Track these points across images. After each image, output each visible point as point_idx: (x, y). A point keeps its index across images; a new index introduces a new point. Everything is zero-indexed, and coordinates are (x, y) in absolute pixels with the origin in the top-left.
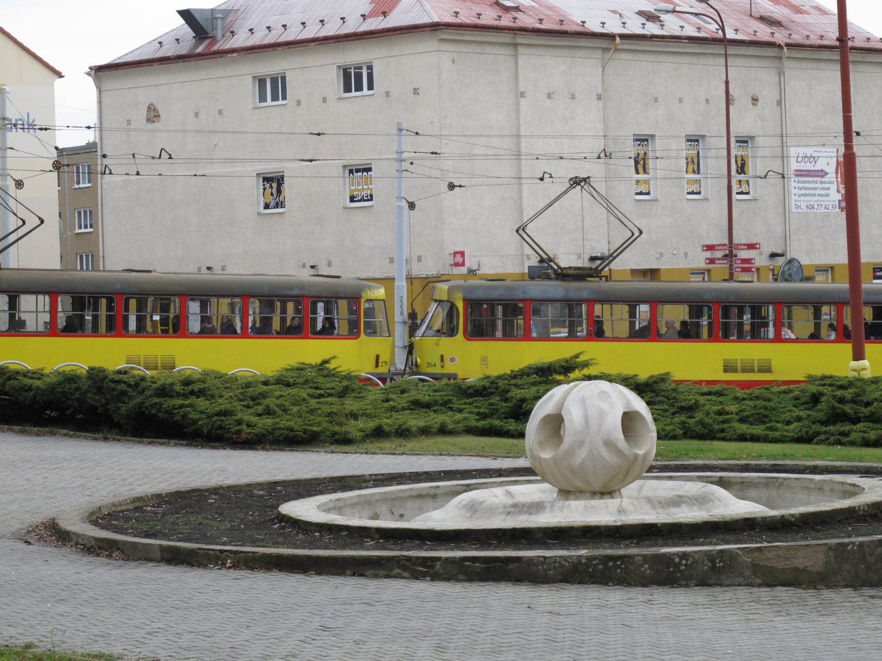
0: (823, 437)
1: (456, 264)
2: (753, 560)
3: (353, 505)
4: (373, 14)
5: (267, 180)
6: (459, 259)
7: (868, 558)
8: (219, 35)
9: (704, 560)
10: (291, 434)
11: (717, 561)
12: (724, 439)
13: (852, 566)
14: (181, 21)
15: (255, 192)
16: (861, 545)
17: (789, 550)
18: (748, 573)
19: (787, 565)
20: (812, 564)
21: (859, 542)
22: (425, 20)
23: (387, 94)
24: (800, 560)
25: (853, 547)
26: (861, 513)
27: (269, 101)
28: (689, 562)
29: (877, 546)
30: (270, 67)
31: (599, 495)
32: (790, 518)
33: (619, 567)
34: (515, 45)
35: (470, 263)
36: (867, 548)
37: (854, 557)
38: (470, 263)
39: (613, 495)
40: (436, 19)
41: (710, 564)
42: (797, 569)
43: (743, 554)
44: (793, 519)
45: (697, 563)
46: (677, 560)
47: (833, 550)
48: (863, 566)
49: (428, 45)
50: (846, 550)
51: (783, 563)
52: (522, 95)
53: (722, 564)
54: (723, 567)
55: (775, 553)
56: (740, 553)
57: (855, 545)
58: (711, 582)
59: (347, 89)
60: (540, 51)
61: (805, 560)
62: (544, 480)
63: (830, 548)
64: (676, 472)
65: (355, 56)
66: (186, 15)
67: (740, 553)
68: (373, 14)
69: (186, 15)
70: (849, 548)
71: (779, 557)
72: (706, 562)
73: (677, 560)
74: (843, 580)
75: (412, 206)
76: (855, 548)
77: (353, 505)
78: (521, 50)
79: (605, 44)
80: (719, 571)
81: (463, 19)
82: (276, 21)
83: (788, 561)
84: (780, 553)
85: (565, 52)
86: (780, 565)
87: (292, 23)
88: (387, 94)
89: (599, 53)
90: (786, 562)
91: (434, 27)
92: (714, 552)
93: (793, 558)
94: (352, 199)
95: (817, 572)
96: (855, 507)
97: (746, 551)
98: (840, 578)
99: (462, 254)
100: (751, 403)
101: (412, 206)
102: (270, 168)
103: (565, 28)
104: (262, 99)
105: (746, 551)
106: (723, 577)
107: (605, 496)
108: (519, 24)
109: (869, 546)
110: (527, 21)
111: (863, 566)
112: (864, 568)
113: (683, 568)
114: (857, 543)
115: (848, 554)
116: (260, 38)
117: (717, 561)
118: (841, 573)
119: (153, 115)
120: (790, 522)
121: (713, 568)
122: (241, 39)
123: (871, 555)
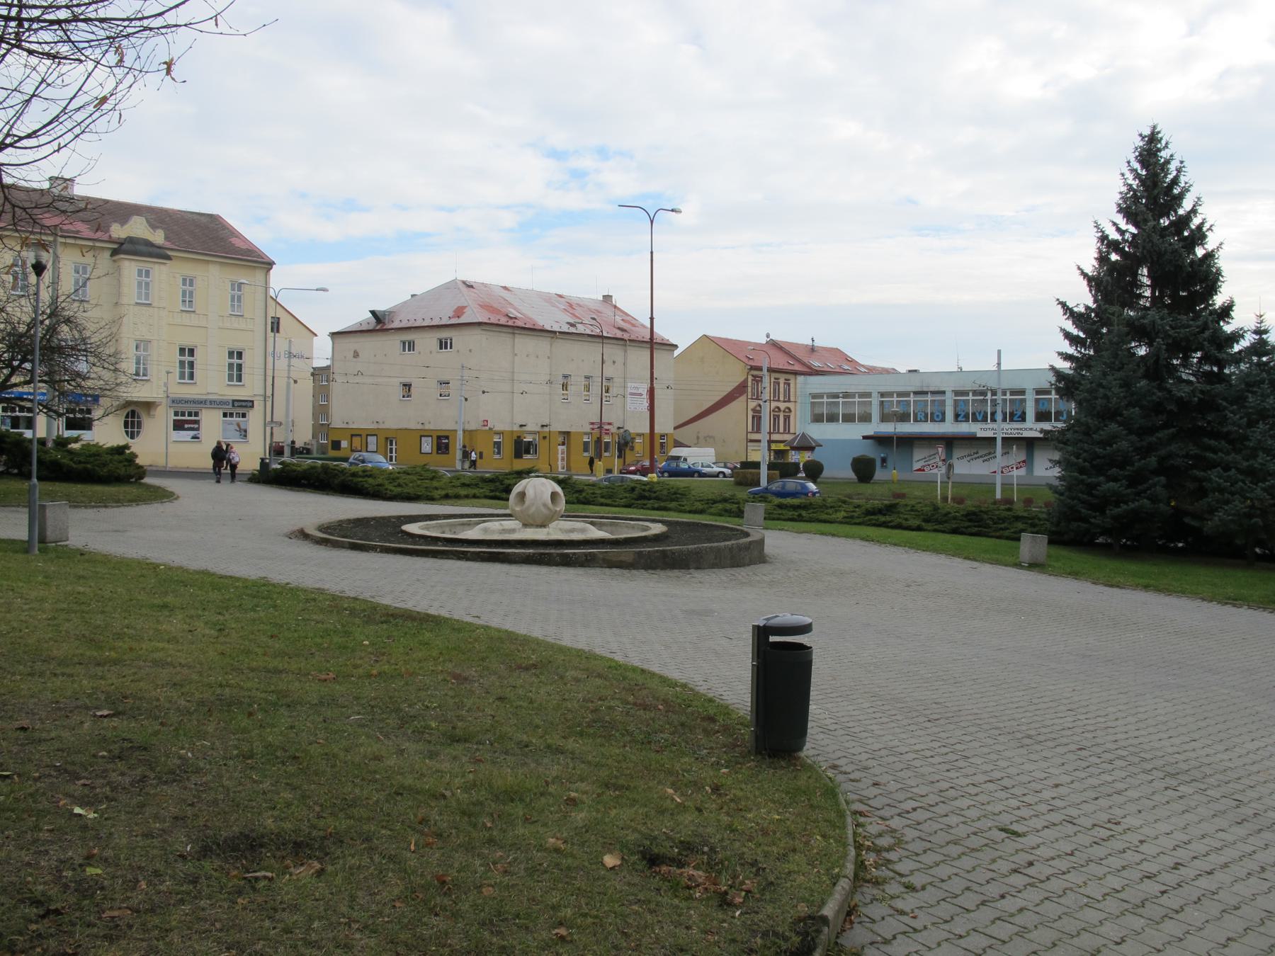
5: (404, 385)
8: (386, 321)
15: (400, 391)
16: (649, 551)
65: (444, 334)
66: (373, 313)
69: (373, 313)
81: (500, 323)
89: (549, 339)
91: (480, 324)
94: (441, 395)
99: (487, 421)
101: (466, 399)
104: (404, 350)
108: (516, 325)
110: (519, 323)
119: (356, 355)
122: (396, 324)
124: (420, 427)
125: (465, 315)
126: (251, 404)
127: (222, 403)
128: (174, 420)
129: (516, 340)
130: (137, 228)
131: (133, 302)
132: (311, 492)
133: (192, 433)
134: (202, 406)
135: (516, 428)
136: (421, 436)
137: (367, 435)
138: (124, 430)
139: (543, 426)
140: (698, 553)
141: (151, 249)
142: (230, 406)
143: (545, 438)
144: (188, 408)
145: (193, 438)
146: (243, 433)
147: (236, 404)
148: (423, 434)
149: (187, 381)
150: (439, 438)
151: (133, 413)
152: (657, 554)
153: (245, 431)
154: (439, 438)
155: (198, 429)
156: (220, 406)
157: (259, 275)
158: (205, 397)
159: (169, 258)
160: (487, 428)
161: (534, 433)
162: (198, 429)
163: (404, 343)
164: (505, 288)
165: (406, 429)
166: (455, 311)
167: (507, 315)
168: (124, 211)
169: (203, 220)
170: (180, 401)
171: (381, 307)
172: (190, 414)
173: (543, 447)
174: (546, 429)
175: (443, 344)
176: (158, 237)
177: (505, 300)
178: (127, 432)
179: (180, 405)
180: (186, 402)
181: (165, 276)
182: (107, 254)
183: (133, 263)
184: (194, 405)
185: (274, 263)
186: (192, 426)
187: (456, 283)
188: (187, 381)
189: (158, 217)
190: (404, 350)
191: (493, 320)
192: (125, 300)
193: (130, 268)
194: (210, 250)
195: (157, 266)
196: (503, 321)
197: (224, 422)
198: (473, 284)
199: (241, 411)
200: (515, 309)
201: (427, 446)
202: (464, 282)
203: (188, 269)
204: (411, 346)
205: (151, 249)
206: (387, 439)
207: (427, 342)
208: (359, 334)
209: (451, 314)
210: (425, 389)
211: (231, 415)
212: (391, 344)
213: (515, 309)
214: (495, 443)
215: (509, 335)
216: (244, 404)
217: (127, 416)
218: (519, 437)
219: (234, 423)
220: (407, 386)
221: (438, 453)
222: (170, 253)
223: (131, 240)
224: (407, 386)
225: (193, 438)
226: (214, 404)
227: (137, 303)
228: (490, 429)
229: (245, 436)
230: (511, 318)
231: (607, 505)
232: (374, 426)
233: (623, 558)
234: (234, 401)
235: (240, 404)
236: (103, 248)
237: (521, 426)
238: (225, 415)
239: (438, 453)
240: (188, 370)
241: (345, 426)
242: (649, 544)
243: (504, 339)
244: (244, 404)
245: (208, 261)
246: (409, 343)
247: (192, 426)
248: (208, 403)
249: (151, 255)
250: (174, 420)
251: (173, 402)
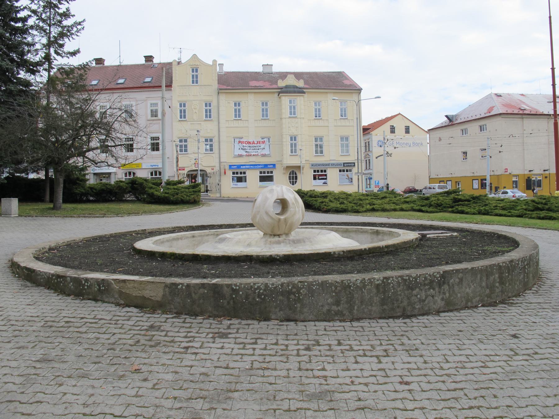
0: (527, 215)
1: (506, 172)
2: (120, 288)
3: (356, 231)
4: (487, 113)
5: (464, 153)
6: (506, 170)
7: (193, 295)
8: (454, 120)
9: (95, 284)
10: (337, 209)
11: (101, 286)
12: (491, 215)
13: (182, 300)
14: (446, 119)
15: (461, 156)
16: (188, 286)
17: (141, 284)
18: (117, 296)
19: (140, 294)
20: (155, 295)
21: (187, 284)
22: (499, 113)
23: (490, 131)
24: (148, 292)
25: (182, 287)
26: (336, 256)
27: (464, 135)
28: (88, 284)
29: (200, 288)
30: (463, 127)
31: (273, 236)
32: (276, 257)
33: (61, 282)
34: (523, 118)
35: (509, 171)
36: (193, 288)
37: (183, 293)
38: (509, 171)
39: (280, 236)
40: (501, 112)
41: (98, 287)
42: (144, 298)
43: (115, 283)
44: (278, 258)
45: (92, 286)
46: (83, 282)
47: (169, 287)
48: (189, 301)
49: (499, 119)
50: (177, 288)
51: (137, 292)
52: (525, 130)
53: (103, 288)
54: (104, 290)
55: (132, 285)
56: (113, 282)
57: (184, 286)
58: (98, 298)
59: (481, 131)
60: (529, 119)
61: (151, 292)
62: (259, 229)
63: (166, 286)
64: (364, 226)
65: (482, 123)
66: (447, 116)
67: (113, 282)
68: (487, 113)
69: (447, 116)
70: (180, 287)
71: (135, 288)
72: (96, 285)
73: (83, 282)
74: (175, 308)
75: (491, 157)
76: (184, 287)
77: (356, 231)
78: (524, 119)
79: (548, 117)
80: (102, 292)
81: (508, 112)
82: (466, 116)
83: (141, 291)
84: (136, 285)
85: (537, 119)
86: (135, 293)
87: (470, 116)
88: (490, 131)
89: (547, 119)
90: (139, 292)
91: (500, 114)
92: (99, 280)
93: (144, 289)
94: (482, 157)
95: (158, 301)
96: (330, 253)
97: (117, 282)
98: (172, 307)
99: (507, 169)
100: (509, 204)
101: (491, 157)
102: (464, 150)
103: (537, 113)
104: (463, 134)
105: (117, 282)
106: (104, 296)
107: (275, 237)
108: (524, 113)
109: (194, 287)
110: (526, 112)
111: (189, 301)
112: (190, 302)
113: (86, 287)
114: (185, 284)
115: (178, 291)
116: (463, 120)
117: (101, 286)
118: (173, 303)
119: (440, 140)
120: (276, 259)
121: (99, 290)
122: (459, 121)
123: (195, 294)
124: (472, 175)
125: (493, 111)
126: (353, 164)
127: (340, 164)
128: (314, 175)
129: (524, 122)
130: (291, 81)
131: (288, 117)
132: (188, 207)
133: (323, 181)
134: (327, 167)
135: (527, 172)
136: (473, 180)
137: (447, 181)
138: (288, 181)
139: (544, 170)
140: (290, 293)
141: (296, 90)
142: (342, 166)
143: (546, 177)
144: (320, 168)
145: (324, 183)
146: (350, 180)
147: (345, 165)
148: (474, 179)
149: (319, 154)
150: (482, 180)
151: (293, 172)
152: (202, 291)
153: (352, 179)
154: (482, 180)
155: (326, 179)
156: (337, 166)
157: (355, 97)
158: (329, 162)
159: (304, 93)
160: (508, 173)
161: (540, 175)
162: (326, 179)
163: (463, 131)
164: (522, 95)
165: (465, 177)
166: (488, 110)
167: (520, 109)
168: (283, 75)
169: (334, 74)
170: (316, 165)
171: (451, 113)
172: (322, 171)
173: (545, 183)
174: (547, 172)
175: (481, 128)
176: (301, 84)
177: (521, 101)
178: (290, 182)
179: (316, 167)
180: (319, 165)
181: (300, 101)
182: (276, 95)
183: (287, 97)
184: (323, 167)
185: (362, 89)
186: (323, 177)
187: (491, 95)
188: (319, 154)
189: (298, 75)
190: (463, 134)
191: (509, 112)
192: (284, 116)
193: (286, 100)
194: (333, 87)
195: (298, 98)
196: (516, 111)
197: (340, 175)
198: (502, 95)
199: (348, 168)
200: (526, 105)
201: (476, 185)
202: (496, 94)
203: (318, 98)
204: (464, 131)
205: (296, 90)
206: (456, 182)
207: (474, 128)
208: (440, 129)
209: (486, 111)
210: (474, 153)
211: (344, 171)
212: (456, 131)
213: (526, 105)
214: (514, 181)
215: (520, 119)
216: (349, 164)
217: (290, 174)
218: (529, 177)
219: (345, 175)
220: (465, 153)
221: (481, 189)
222: (305, 90)
223: (287, 87)
224: (465, 153)
225: (324, 183)
226: (334, 165)
227: (290, 117)
228: (510, 174)
229: (352, 181)
230: (522, 110)
231: (505, 216)
232: (450, 176)
233: (147, 293)
234: (344, 163)
235: (348, 164)
236: (274, 92)
237: (530, 171)
238: (340, 171)
239: (481, 189)
240: (319, 149)
241: (437, 177)
242: (337, 266)
243: (517, 121)
244: (349, 164)
245: (327, 92)
246: (465, 130)
247: (323, 177)
248: (330, 165)
249: (295, 92)
250: (314, 175)
251: (312, 165)
